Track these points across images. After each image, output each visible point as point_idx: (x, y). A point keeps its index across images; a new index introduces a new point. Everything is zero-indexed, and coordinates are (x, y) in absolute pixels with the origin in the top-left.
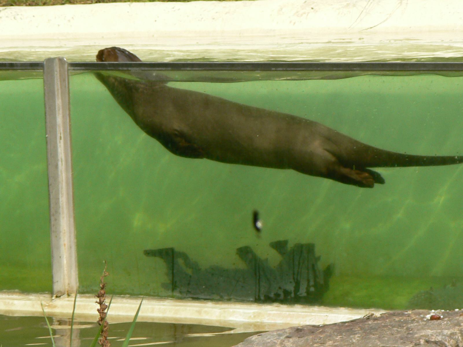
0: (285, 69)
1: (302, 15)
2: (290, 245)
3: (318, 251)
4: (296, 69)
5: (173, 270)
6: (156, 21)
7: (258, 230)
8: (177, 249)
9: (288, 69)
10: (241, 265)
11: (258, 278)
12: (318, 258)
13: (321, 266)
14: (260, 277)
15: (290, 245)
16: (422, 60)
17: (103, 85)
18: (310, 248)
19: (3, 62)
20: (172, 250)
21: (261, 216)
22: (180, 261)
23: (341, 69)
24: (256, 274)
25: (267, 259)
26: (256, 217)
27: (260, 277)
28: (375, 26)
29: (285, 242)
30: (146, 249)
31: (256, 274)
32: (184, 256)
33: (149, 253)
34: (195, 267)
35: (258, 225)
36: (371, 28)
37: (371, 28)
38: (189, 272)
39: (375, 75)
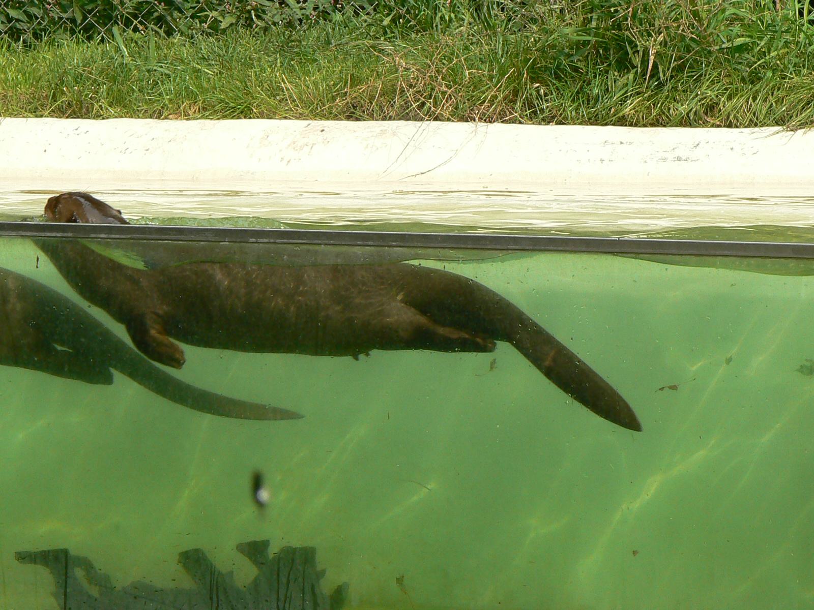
0: (272, 241)
1: (301, 148)
2: (273, 550)
3: (322, 560)
4: (291, 241)
5: (66, 587)
6: (45, 151)
7: (260, 504)
8: (73, 552)
9: (278, 241)
10: (187, 583)
11: (215, 604)
12: (323, 573)
13: (326, 587)
14: (218, 603)
15: (273, 550)
16: (552, 232)
17: (549, 255)
18: (307, 556)
19: (220, 228)
20: (65, 552)
21: (272, 478)
22: (79, 573)
23: (370, 243)
24: (211, 599)
25: (232, 572)
26: (257, 483)
27: (218, 603)
28: (429, 171)
29: (265, 544)
30: (20, 549)
31: (211, 599)
32: (87, 565)
33: (24, 557)
34: (103, 583)
35: (263, 494)
36: (422, 173)
37: (422, 173)
38: (94, 592)
39: (534, 253)
